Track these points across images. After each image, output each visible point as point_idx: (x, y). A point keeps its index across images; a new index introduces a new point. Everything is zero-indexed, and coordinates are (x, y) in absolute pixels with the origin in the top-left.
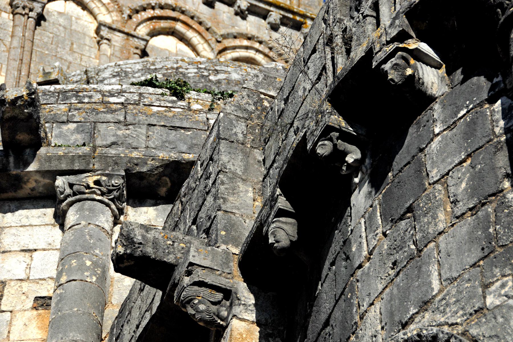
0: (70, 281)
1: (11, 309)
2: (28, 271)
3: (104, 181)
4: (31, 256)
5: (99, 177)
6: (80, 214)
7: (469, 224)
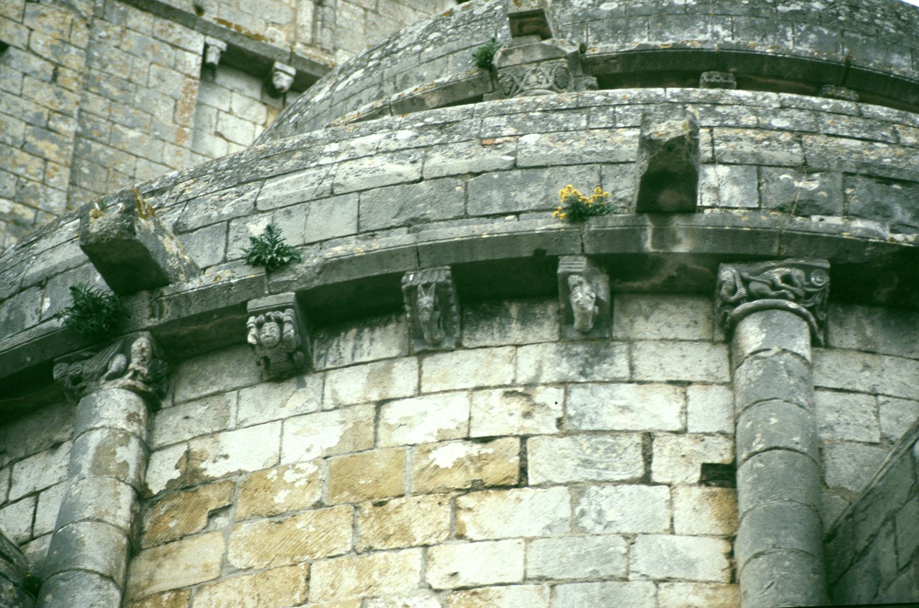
0: (771, 449)
1: (668, 480)
2: (683, 418)
3: (798, 277)
4: (685, 393)
5: (788, 270)
6: (767, 333)
7: (536, 152)
